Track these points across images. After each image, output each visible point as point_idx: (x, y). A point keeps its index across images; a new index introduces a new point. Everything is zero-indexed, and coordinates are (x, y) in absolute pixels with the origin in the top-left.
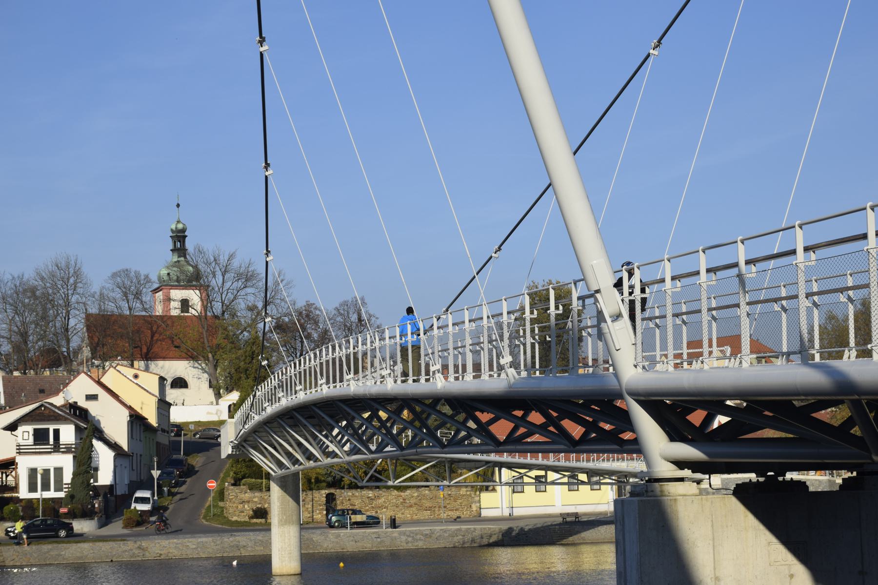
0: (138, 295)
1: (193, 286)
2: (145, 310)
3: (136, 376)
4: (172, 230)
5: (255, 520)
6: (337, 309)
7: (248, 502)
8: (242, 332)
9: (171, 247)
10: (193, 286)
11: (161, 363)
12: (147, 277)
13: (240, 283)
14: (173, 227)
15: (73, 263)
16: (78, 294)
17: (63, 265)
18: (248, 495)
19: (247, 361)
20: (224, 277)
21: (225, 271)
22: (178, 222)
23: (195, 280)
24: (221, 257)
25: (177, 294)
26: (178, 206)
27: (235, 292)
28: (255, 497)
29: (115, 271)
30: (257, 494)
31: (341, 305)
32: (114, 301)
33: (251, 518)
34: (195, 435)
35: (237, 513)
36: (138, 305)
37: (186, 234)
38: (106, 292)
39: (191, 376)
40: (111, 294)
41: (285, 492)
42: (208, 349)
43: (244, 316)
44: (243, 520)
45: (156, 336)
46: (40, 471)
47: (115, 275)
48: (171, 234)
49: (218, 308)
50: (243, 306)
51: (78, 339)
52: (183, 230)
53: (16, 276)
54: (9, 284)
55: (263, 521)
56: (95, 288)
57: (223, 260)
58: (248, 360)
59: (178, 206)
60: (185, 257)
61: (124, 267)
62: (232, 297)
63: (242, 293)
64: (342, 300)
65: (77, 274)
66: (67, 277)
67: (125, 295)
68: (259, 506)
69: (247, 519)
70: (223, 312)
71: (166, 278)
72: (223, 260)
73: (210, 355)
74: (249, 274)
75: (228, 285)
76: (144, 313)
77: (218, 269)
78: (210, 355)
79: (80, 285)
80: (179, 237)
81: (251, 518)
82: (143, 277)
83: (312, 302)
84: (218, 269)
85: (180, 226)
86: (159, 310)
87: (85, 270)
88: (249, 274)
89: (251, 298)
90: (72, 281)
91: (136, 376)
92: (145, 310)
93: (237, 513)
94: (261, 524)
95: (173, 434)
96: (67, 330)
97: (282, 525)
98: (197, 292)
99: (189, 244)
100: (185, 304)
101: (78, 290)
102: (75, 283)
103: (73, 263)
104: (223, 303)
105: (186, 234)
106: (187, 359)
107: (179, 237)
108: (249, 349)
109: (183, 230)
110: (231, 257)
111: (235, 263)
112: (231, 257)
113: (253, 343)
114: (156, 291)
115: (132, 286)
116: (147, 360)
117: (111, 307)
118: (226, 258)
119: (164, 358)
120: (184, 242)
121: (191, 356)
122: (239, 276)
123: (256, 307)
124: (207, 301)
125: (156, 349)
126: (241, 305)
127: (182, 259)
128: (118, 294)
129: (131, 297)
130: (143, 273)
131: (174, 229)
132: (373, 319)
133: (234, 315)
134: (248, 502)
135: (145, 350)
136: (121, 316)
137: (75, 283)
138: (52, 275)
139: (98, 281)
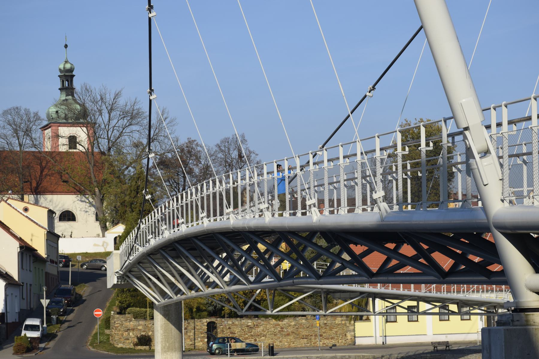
0: (28, 132)
2: (35, 146)
4: (60, 70)
5: (139, 347)
7: (133, 330)
10: (81, 123)
11: (49, 197)
13: (126, 121)
14: (62, 67)
18: (133, 323)
19: (133, 196)
21: (111, 109)
22: (66, 62)
23: (81, 117)
24: (108, 96)
25: (65, 131)
26: (66, 46)
27: (121, 129)
28: (139, 325)
29: (5, 109)
30: (142, 322)
31: (222, 142)
33: (136, 345)
34: (82, 266)
35: (122, 340)
36: (28, 141)
37: (74, 73)
41: (168, 320)
42: (95, 184)
44: (128, 347)
45: (46, 172)
47: (5, 113)
48: (60, 74)
49: (104, 144)
50: (128, 142)
52: (71, 70)
55: (147, 348)
57: (109, 98)
59: (66, 46)
63: (128, 130)
64: (223, 137)
67: (16, 131)
68: (143, 333)
69: (132, 346)
70: (109, 149)
71: (54, 116)
72: (109, 98)
73: (97, 190)
74: (135, 112)
75: (113, 123)
77: (104, 107)
80: (67, 76)
81: (136, 345)
82: (32, 115)
83: (193, 139)
84: (104, 107)
85: (68, 66)
86: (48, 147)
88: (135, 112)
89: (136, 135)
91: (26, 210)
92: (35, 146)
93: (122, 340)
94: (145, 351)
95: (61, 265)
97: (165, 352)
98: (85, 129)
99: (77, 83)
100: (73, 141)
104: (109, 140)
105: (74, 73)
107: (67, 76)
109: (71, 70)
110: (117, 95)
111: (121, 102)
112: (117, 95)
113: (138, 178)
116: (37, 194)
119: (52, 192)
120: (72, 81)
121: (79, 191)
122: (124, 114)
125: (45, 184)
126: (127, 141)
129: (21, 134)
131: (62, 69)
132: (253, 155)
133: (119, 152)
134: (133, 330)
135: (34, 185)
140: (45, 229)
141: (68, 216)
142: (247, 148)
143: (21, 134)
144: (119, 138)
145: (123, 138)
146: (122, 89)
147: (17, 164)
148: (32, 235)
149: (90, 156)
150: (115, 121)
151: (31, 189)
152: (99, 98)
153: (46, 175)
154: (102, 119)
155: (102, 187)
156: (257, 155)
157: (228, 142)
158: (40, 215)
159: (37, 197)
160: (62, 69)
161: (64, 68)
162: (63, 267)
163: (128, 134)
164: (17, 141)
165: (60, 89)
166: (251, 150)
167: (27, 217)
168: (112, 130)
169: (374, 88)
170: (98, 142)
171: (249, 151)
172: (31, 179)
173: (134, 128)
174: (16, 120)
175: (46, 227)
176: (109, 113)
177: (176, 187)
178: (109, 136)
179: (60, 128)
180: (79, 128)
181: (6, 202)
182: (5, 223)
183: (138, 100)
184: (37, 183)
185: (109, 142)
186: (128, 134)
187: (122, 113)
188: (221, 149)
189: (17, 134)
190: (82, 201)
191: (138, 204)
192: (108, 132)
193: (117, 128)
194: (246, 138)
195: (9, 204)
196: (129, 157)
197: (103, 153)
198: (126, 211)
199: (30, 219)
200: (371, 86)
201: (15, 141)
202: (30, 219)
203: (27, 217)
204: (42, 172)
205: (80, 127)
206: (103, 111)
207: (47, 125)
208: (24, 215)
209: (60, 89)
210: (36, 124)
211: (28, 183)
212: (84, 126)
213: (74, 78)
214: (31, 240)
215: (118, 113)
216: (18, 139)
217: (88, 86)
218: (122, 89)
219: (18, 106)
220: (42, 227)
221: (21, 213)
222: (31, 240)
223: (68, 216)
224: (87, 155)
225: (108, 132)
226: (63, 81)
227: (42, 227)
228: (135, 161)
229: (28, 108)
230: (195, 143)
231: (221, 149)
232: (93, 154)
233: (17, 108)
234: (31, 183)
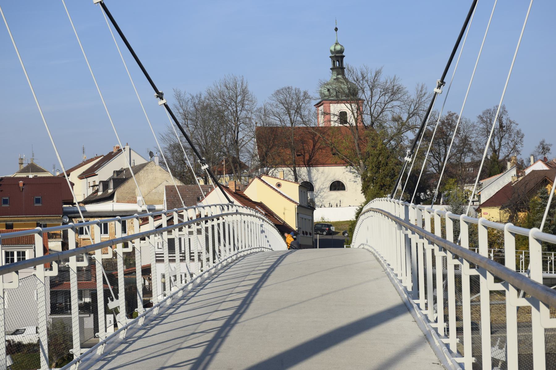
0: (298, 110)
1: (344, 100)
2: (304, 122)
3: (279, 185)
4: (331, 51)
6: (481, 118)
8: (389, 141)
9: (331, 66)
10: (344, 100)
11: (321, 169)
12: (305, 93)
13: (387, 98)
14: (332, 48)
15: (239, 83)
16: (246, 110)
17: (231, 85)
19: (375, 171)
20: (372, 92)
22: (337, 44)
23: (351, 95)
24: (369, 75)
25: (336, 108)
26: (336, 29)
27: (383, 105)
31: (484, 113)
32: (278, 115)
34: (344, 234)
36: (299, 118)
37: (344, 54)
38: (269, 107)
39: (348, 180)
40: (275, 110)
42: (359, 156)
43: (391, 127)
45: (318, 145)
46: (115, 299)
47: (278, 93)
48: (331, 55)
49: (367, 120)
50: (390, 117)
51: (249, 147)
52: (341, 51)
53: (195, 96)
54: (190, 102)
56: (260, 103)
57: (370, 76)
58: (375, 169)
59: (336, 29)
60: (343, 74)
61: (286, 86)
62: (380, 110)
63: (389, 106)
64: (484, 109)
65: (244, 92)
66: (237, 96)
67: (288, 110)
70: (373, 123)
71: (327, 93)
72: (370, 76)
73: (361, 162)
74: (395, 88)
75: (375, 99)
76: (304, 126)
77: (366, 85)
78: (361, 162)
79: (246, 102)
80: (338, 57)
82: (302, 94)
83: (453, 112)
84: (366, 85)
85: (338, 48)
86: (321, 122)
87: (251, 89)
88: (395, 88)
89: (397, 110)
90: (239, 98)
91: (279, 185)
92: (304, 122)
95: (325, 233)
96: (237, 142)
98: (348, 105)
99: (346, 62)
100: (343, 116)
101: (246, 107)
102: (243, 100)
103: (239, 83)
104: (371, 115)
105: (344, 54)
106: (344, 164)
107: (338, 57)
108: (375, 159)
109: (341, 51)
110: (377, 74)
111: (382, 79)
112: (377, 74)
113: (379, 154)
114: (318, 105)
115: (293, 102)
116: (309, 166)
117: (275, 121)
118: (373, 75)
119: (324, 164)
120: (342, 61)
121: (346, 162)
122: (385, 91)
123: (401, 118)
124: (360, 112)
125: (317, 156)
126: (388, 115)
127: (340, 76)
128: (281, 109)
129: (292, 112)
130: (302, 90)
131: (333, 50)
132: (513, 125)
133: (381, 126)
135: (307, 157)
136: (284, 128)
137: (243, 100)
138: (222, 95)
139: (263, 100)
140: (296, 203)
141: (337, 186)
142: (508, 119)
143: (292, 112)
144: (381, 113)
145: (385, 113)
146: (382, 68)
147: (289, 139)
148: (285, 209)
149: (355, 131)
150: (377, 97)
151: (304, 162)
152: (360, 75)
153: (319, 148)
154: (365, 95)
155: (366, 159)
156: (517, 124)
157: (490, 113)
158: (292, 190)
159: (310, 169)
160: (333, 50)
161: (335, 49)
162: (327, 234)
163: (390, 109)
164: (289, 119)
165: (331, 69)
166: (512, 120)
167: (279, 192)
168: (374, 105)
169: (442, 82)
170: (362, 117)
171: (510, 121)
172: (304, 153)
173: (395, 103)
174: (287, 99)
175: (298, 202)
176: (371, 90)
177: (437, 157)
178: (372, 111)
179: (331, 105)
180: (343, 105)
181: (260, 178)
182: (251, 198)
183: (397, 78)
184: (310, 156)
185: (372, 117)
186: (390, 109)
187: (382, 90)
188: (483, 120)
189: (288, 111)
190: (350, 172)
191: (380, 180)
192: (370, 108)
193: (379, 104)
194: (506, 110)
195: (262, 180)
196: (389, 131)
197: (366, 127)
198: (368, 186)
199: (281, 194)
200: (439, 80)
201: (287, 118)
202: (281, 194)
203: (279, 192)
204: (314, 146)
205: (344, 103)
206: (365, 89)
207: (320, 103)
208: (276, 190)
209: (331, 69)
210: (306, 102)
211: (302, 157)
212: (347, 103)
213: (344, 58)
214: (284, 214)
215: (379, 90)
216: (290, 116)
217: (350, 67)
218: (382, 68)
219: (290, 86)
220: (293, 202)
221: (274, 189)
222: (284, 214)
223: (337, 186)
224: (352, 130)
225: (370, 108)
226: (334, 62)
227: (293, 202)
228: (396, 135)
229: (298, 88)
230: (455, 115)
231: (483, 120)
232: (357, 129)
233: (289, 88)
234: (304, 156)
